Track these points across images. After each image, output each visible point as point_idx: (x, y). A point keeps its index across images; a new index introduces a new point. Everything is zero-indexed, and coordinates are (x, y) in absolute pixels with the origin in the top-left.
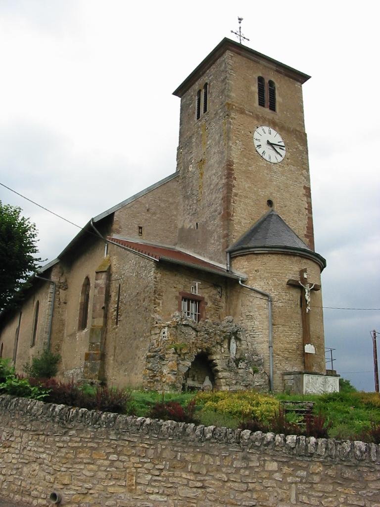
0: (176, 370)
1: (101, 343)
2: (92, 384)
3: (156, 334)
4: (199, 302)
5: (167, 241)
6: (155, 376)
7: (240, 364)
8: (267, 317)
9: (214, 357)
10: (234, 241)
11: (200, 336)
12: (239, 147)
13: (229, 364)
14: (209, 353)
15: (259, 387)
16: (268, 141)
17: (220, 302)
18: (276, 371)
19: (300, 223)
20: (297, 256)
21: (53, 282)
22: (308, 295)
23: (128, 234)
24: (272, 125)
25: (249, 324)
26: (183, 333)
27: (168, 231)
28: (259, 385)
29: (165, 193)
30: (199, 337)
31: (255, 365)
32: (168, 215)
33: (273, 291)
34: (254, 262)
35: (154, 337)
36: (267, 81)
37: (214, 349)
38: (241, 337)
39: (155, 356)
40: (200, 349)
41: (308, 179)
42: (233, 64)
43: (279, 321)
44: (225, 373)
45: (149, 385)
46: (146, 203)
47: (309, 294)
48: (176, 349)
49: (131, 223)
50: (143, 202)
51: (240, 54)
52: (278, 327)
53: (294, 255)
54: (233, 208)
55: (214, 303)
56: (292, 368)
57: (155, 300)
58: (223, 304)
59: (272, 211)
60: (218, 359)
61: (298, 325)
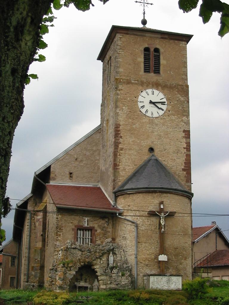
0: (62, 277)
1: (41, 258)
2: (33, 286)
3: (56, 255)
4: (91, 230)
5: (92, 180)
6: (52, 281)
7: (114, 270)
8: (134, 238)
9: (95, 267)
10: (120, 183)
11: (84, 254)
12: (125, 112)
13: (106, 270)
14: (92, 264)
15: (125, 285)
16: (150, 101)
17: (107, 228)
18: (140, 274)
19: (178, 160)
20: (157, 192)
21: (29, 211)
22: (162, 221)
23: (62, 180)
24: (155, 86)
25: (124, 243)
26: (72, 253)
27: (92, 172)
28: (125, 284)
29: (89, 143)
30: (83, 255)
31: (124, 271)
32: (93, 160)
33: (139, 219)
34: (127, 200)
35: (55, 257)
36: (152, 50)
37: (95, 262)
38: (117, 253)
39: (53, 269)
40: (82, 263)
41: (188, 123)
42: (121, 44)
43: (142, 239)
44: (102, 277)
45: (49, 287)
46: (74, 154)
47: (163, 220)
48: (64, 264)
49: (64, 171)
50: (72, 154)
51: (127, 34)
52: (142, 244)
53: (155, 192)
54: (119, 160)
55: (102, 230)
56: (151, 271)
57: (57, 233)
58: (110, 230)
59: (153, 155)
60: (98, 268)
61: (156, 242)
